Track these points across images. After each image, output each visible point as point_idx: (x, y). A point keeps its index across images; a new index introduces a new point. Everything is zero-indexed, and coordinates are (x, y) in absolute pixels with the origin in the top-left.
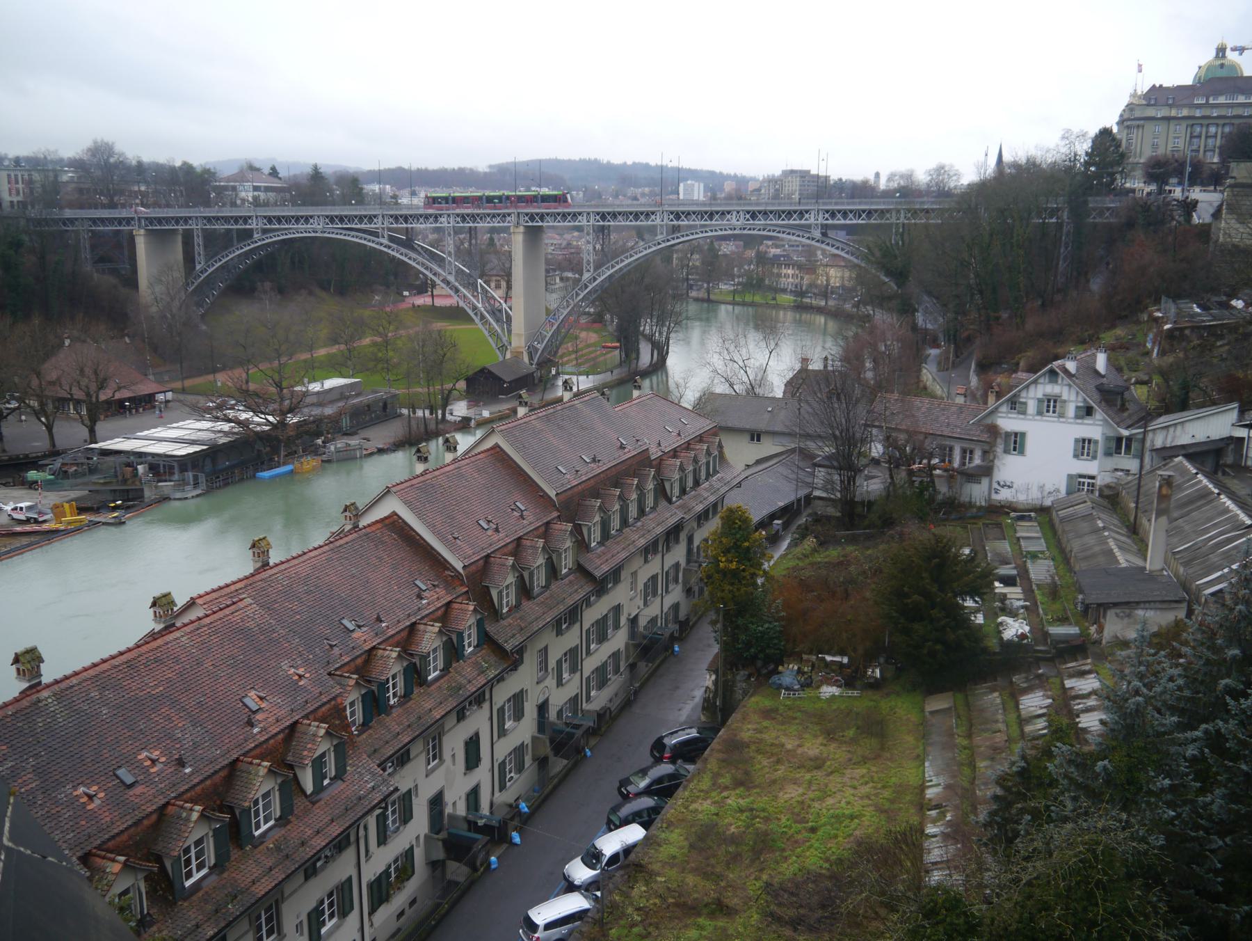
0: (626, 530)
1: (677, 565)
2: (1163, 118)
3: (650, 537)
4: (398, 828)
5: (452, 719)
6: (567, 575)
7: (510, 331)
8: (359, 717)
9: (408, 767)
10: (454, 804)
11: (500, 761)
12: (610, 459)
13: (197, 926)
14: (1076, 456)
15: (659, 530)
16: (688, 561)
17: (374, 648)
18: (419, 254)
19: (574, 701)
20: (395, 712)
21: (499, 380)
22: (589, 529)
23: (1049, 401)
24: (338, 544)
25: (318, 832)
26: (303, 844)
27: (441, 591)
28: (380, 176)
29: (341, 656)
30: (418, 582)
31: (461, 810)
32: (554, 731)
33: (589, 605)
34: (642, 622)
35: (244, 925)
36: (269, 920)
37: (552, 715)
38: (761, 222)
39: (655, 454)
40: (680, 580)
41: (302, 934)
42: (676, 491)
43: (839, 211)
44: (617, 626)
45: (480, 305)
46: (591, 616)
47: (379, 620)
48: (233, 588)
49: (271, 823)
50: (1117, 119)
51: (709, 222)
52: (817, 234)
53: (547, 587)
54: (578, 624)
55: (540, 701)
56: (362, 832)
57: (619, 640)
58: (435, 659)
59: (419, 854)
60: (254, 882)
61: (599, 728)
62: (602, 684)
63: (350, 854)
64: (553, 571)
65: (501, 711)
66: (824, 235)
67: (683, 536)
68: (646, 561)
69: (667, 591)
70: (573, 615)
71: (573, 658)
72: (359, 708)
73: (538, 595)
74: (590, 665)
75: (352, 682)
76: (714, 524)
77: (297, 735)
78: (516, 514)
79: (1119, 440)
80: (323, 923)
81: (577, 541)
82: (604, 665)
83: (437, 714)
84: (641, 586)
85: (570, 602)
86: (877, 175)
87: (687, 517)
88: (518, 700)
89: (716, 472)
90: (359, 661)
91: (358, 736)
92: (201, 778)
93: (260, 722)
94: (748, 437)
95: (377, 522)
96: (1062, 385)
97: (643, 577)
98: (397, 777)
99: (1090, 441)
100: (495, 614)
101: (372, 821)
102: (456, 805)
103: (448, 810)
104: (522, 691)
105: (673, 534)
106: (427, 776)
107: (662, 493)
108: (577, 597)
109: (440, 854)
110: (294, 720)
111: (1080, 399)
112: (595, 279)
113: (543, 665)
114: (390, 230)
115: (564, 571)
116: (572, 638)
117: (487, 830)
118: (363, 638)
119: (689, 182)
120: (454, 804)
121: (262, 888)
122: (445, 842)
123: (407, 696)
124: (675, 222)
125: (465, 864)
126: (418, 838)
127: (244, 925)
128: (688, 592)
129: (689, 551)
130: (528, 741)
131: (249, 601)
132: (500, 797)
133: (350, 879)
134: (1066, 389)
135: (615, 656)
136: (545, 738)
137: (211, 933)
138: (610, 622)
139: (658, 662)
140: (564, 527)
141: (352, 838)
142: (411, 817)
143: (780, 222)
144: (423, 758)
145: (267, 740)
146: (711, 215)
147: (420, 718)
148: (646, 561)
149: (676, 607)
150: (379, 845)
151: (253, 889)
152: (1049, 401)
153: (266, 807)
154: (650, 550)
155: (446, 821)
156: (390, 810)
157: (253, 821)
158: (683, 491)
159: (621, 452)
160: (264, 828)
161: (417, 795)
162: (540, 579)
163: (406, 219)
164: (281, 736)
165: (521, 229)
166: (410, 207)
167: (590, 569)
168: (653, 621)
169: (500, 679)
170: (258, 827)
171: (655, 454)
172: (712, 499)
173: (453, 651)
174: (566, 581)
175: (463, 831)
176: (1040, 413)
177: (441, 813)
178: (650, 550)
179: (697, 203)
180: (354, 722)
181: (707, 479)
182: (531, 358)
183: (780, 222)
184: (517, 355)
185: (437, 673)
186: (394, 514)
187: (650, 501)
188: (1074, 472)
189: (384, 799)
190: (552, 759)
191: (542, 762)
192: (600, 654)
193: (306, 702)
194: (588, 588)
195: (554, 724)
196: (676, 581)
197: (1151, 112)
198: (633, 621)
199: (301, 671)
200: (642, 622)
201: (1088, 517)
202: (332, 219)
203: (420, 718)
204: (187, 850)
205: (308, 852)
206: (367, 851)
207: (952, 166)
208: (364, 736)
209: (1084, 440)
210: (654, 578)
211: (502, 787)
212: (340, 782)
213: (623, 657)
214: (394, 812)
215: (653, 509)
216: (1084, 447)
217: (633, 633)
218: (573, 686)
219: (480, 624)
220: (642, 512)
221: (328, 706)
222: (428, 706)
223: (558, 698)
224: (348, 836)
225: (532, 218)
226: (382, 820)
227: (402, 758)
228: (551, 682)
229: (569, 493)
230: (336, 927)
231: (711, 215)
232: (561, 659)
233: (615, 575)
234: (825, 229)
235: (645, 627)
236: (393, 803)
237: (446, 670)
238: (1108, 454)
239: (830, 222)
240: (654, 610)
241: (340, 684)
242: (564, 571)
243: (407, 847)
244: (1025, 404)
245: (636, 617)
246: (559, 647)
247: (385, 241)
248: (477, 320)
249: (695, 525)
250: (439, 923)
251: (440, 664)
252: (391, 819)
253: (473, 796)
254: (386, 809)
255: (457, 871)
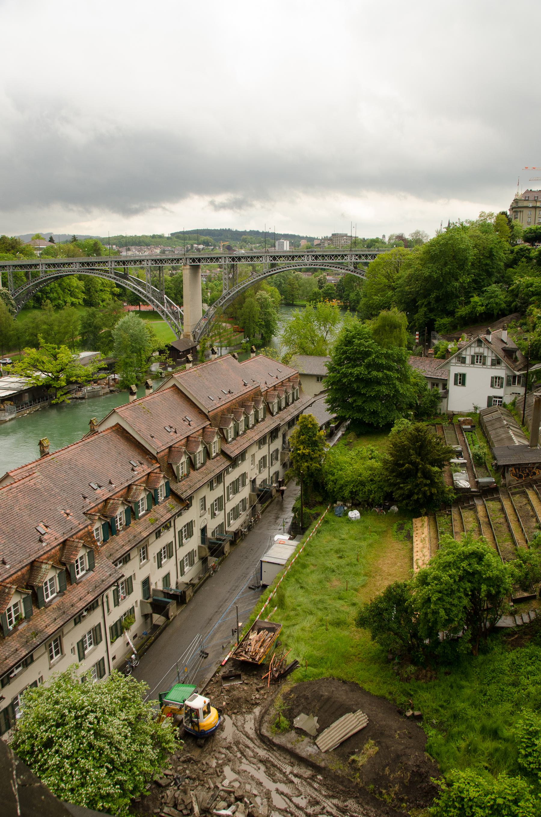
0: (209, 463)
1: (277, 450)
2: (533, 207)
3: (261, 435)
4: (125, 597)
5: (153, 536)
6: (215, 457)
7: (182, 324)
8: (101, 537)
9: (130, 564)
10: (156, 583)
11: (181, 560)
12: (239, 391)
13: (17, 650)
14: (492, 386)
15: (267, 430)
16: (283, 448)
17: (108, 499)
18: (132, 282)
19: (221, 526)
20: (122, 533)
21: (178, 351)
22: (227, 431)
23: (477, 356)
24: (86, 441)
25: (80, 599)
26: (72, 606)
27: (145, 467)
28: (108, 241)
29: (90, 504)
30: (132, 462)
31: (160, 587)
32: (211, 543)
33: (228, 473)
34: (258, 482)
35: (42, 649)
36: (56, 646)
37: (209, 534)
38: (320, 261)
39: (263, 388)
40: (279, 458)
41: (74, 654)
42: (276, 409)
43: (363, 255)
44: (244, 485)
45: (165, 310)
46: (229, 479)
47: (110, 483)
48: (30, 467)
49: (55, 594)
50: (509, 208)
51: (292, 262)
52: (352, 268)
53: (203, 464)
54: (222, 484)
55: (202, 527)
56: (105, 599)
57: (245, 492)
58: (142, 504)
59: (137, 611)
60: (46, 627)
61: (235, 541)
62: (236, 517)
63: (98, 611)
64: (207, 454)
65: (181, 532)
66: (355, 268)
67: (280, 434)
68: (260, 448)
69: (272, 465)
70: (219, 478)
71: (220, 503)
72: (101, 531)
73: (200, 468)
74: (229, 506)
75: (97, 518)
76: (296, 428)
77: (67, 547)
78: (187, 423)
79: (514, 377)
80: (86, 648)
81: (221, 437)
82: (237, 506)
83: (145, 534)
84: (257, 462)
85: (217, 471)
86: (384, 236)
87: (282, 423)
88: (190, 526)
89: (298, 399)
90: (100, 506)
91: (101, 547)
92: (15, 571)
93: (46, 540)
94: (316, 379)
95: (108, 429)
96: (484, 348)
97: (258, 458)
98: (123, 569)
99: (499, 378)
100: (175, 478)
101: (110, 593)
102: (157, 584)
103: (153, 587)
104: (192, 521)
105: (274, 434)
106: (50, 669)
107: (268, 410)
108: (221, 469)
109: (149, 610)
110: (33, 559)
111: (493, 355)
112: (229, 294)
113: (204, 507)
114: (115, 269)
115: (214, 455)
116: (219, 491)
117: (173, 597)
118: (103, 493)
119: (281, 241)
120: (156, 583)
121: (50, 630)
122: (151, 604)
123: (128, 524)
124: (273, 262)
125: (163, 615)
126: (136, 602)
127: (42, 649)
128: (284, 465)
129: (284, 442)
130: (196, 548)
131: (38, 474)
132: (182, 579)
133: (99, 625)
134: (486, 350)
135: (243, 501)
136: (206, 547)
137: (24, 654)
138: (240, 482)
139: (266, 504)
140: (213, 430)
141: (100, 603)
142: (132, 591)
143: (331, 261)
144: (138, 558)
145: (50, 550)
146: (293, 257)
147: (135, 537)
148: (260, 448)
149: (277, 474)
150: (115, 606)
151: (46, 630)
152: (477, 356)
153: (52, 586)
154: (262, 442)
155: (151, 593)
156: (120, 587)
157: (45, 594)
158: (280, 409)
159: (244, 388)
160: (51, 597)
161: (135, 579)
162: (200, 459)
163: (124, 263)
164: (58, 547)
165: (188, 267)
166: (126, 257)
167: (228, 453)
168: (264, 481)
169: (179, 514)
170: (47, 596)
171: (263, 388)
172: (296, 413)
173: (153, 500)
174: (215, 460)
175: (161, 598)
176: (473, 363)
177: (149, 588)
178: (262, 442)
179: (286, 252)
180: (98, 540)
181: (293, 403)
182: (194, 338)
183: (331, 261)
184: (187, 336)
185: (144, 512)
186: (118, 424)
187: (261, 415)
188: (491, 395)
189: (117, 581)
190: (209, 558)
191: (204, 560)
192: (235, 501)
193: (72, 529)
194: (228, 463)
195: (210, 539)
196: (277, 459)
197: (525, 204)
198: (253, 482)
199: (68, 511)
200: (258, 482)
201: (499, 419)
202: (83, 264)
203: (135, 537)
204: (9, 610)
205: (76, 610)
206: (108, 610)
207: (424, 232)
208: (105, 547)
209: (496, 378)
210: (264, 458)
211: (182, 573)
212: (92, 572)
213: (248, 501)
214: (122, 588)
215: (263, 420)
216: (496, 381)
217: (253, 489)
218: (220, 518)
219: (167, 484)
220: (257, 421)
221: (83, 531)
222: (139, 530)
223: (212, 525)
224: (97, 601)
225: (194, 260)
226: (116, 592)
227: (125, 559)
228: (208, 516)
229: (215, 411)
230: (94, 650)
231: (293, 257)
232: (213, 504)
233: (242, 456)
234: (356, 265)
235: (260, 485)
236: (122, 583)
237: (148, 511)
238: (509, 384)
239: (359, 261)
240: (265, 475)
241: (90, 519)
242: (214, 455)
243: (131, 607)
244: (465, 358)
245: (255, 479)
246: (212, 496)
247: (113, 276)
248: (164, 317)
249: (287, 428)
250: (149, 647)
251: (146, 507)
252: (121, 592)
253: (166, 579)
254: (118, 586)
255: (158, 619)
